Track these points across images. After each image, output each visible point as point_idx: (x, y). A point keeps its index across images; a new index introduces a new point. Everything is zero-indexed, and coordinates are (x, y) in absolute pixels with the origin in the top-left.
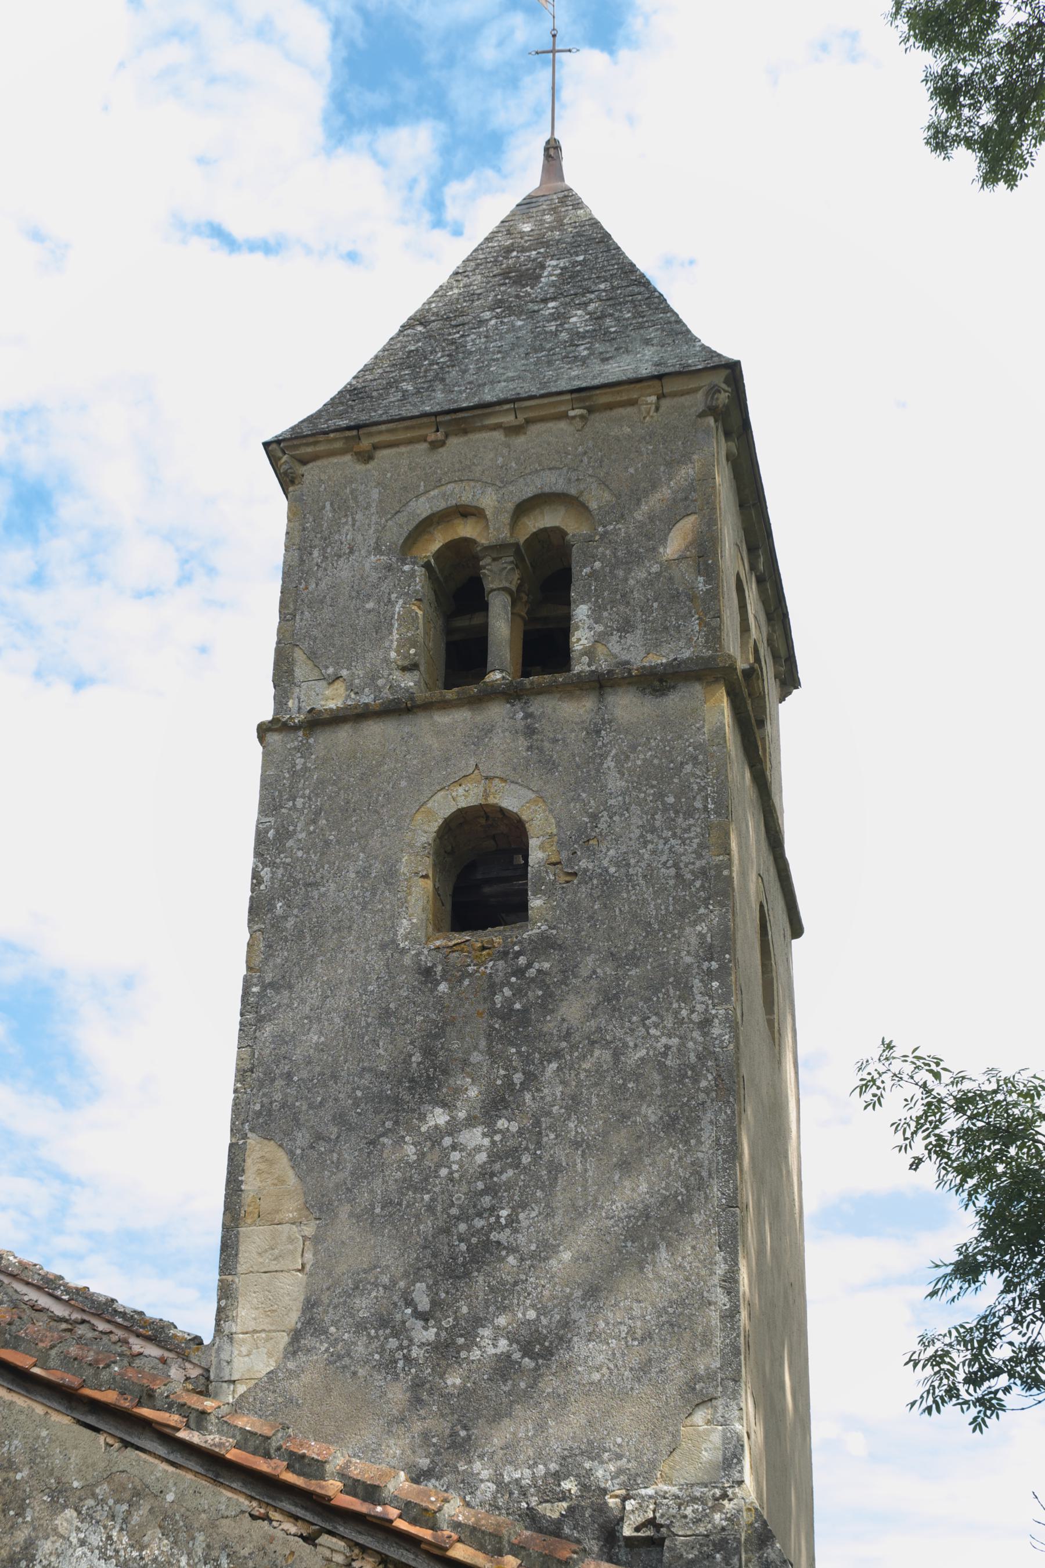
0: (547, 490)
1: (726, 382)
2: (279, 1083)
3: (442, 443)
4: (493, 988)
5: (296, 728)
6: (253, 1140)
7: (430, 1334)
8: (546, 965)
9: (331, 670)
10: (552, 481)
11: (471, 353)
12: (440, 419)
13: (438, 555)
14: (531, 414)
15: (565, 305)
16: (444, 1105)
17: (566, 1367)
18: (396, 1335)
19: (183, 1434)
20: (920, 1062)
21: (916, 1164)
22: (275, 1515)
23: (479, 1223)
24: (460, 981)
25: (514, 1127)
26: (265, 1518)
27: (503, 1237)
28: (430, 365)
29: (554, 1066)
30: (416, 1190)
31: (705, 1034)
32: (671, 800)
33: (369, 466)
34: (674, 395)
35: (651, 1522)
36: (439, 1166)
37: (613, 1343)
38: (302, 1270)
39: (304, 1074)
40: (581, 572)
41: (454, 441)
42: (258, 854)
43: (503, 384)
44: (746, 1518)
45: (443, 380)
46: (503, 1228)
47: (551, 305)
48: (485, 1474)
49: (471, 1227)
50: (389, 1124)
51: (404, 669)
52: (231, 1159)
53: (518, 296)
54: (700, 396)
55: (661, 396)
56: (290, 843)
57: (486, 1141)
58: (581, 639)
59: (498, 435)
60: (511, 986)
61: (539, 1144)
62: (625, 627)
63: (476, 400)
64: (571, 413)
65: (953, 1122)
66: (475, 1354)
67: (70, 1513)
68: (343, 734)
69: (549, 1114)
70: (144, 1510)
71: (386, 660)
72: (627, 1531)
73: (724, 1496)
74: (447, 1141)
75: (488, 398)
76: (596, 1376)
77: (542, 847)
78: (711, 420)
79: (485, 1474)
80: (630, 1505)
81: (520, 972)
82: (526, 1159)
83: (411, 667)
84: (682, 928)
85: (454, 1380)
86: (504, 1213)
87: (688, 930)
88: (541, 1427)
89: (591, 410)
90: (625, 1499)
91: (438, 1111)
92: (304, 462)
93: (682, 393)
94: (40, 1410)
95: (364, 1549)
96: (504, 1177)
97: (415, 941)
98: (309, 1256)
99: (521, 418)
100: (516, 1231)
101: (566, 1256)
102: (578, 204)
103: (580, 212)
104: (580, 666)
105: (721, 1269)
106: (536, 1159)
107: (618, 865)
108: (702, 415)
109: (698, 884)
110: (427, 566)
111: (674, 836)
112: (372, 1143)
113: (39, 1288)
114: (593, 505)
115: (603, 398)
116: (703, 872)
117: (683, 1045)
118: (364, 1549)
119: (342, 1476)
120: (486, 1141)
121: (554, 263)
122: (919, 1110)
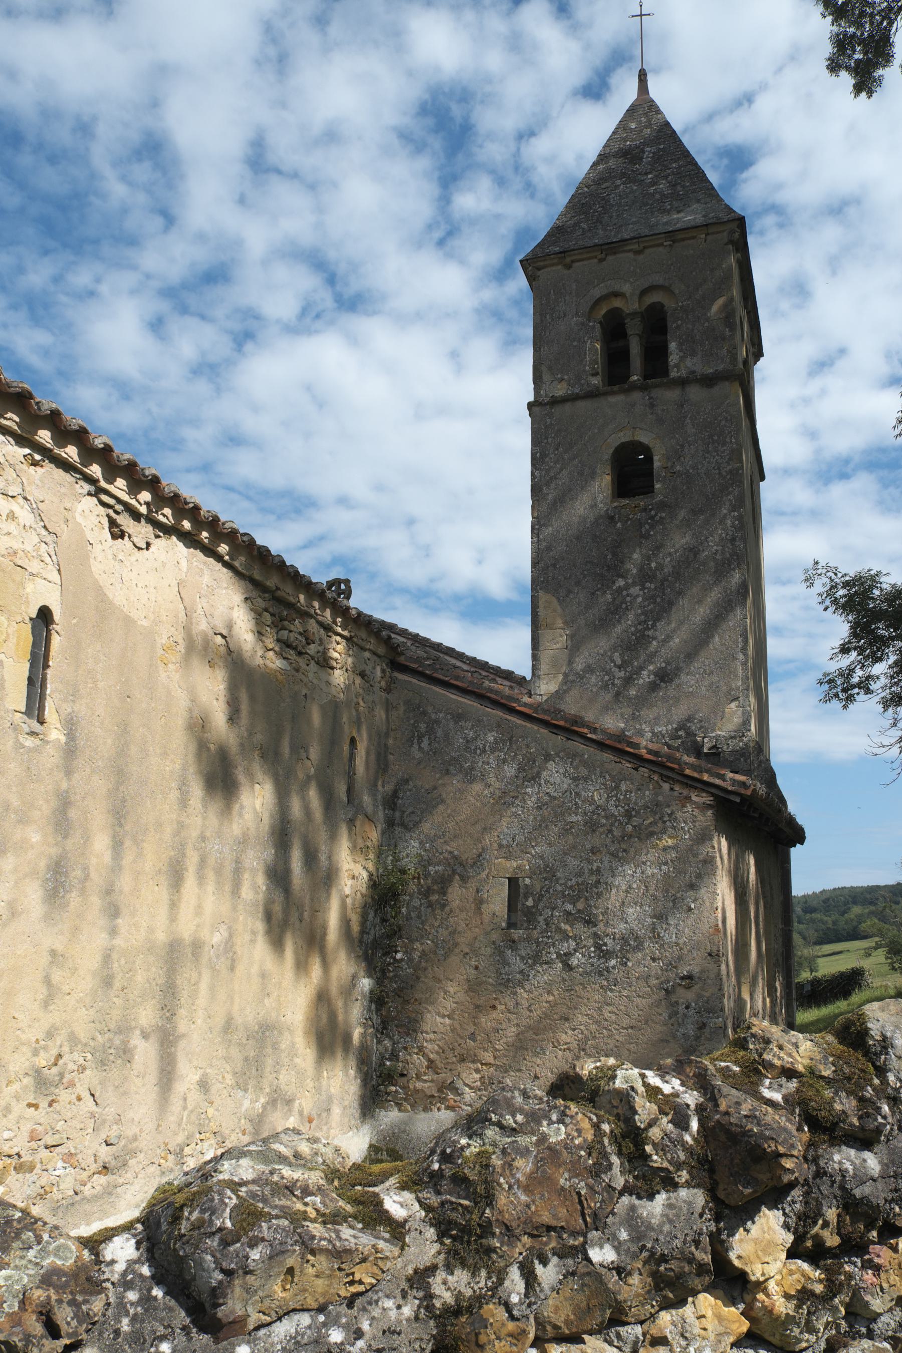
0: (655, 283)
1: (738, 227)
2: (551, 568)
3: (604, 260)
4: (641, 525)
5: (546, 404)
6: (541, 594)
7: (622, 674)
8: (664, 515)
9: (559, 376)
10: (658, 279)
11: (613, 206)
12: (603, 247)
13: (605, 316)
14: (646, 244)
15: (656, 176)
16: (622, 577)
17: (679, 686)
18: (607, 674)
19: (589, 736)
20: (828, 568)
21: (826, 609)
22: (623, 762)
23: (640, 627)
24: (626, 522)
25: (653, 586)
26: (620, 762)
27: (650, 633)
28: (594, 212)
29: (669, 559)
30: (612, 613)
31: (732, 545)
32: (716, 438)
33: (570, 271)
34: (713, 233)
35: (714, 747)
36: (622, 603)
37: (697, 676)
38: (566, 648)
39: (562, 564)
40: (672, 325)
41: (610, 258)
42: (533, 465)
43: (631, 226)
44: (751, 744)
45: (601, 222)
46: (650, 629)
47: (650, 176)
48: (647, 729)
49: (636, 629)
50: (599, 586)
51: (593, 375)
52: (532, 602)
53: (632, 171)
54: (725, 234)
55: (707, 234)
56: (547, 459)
57: (641, 593)
58: (673, 359)
59: (631, 255)
60: (649, 524)
61: (664, 594)
62: (693, 354)
63: (619, 237)
64: (665, 244)
65: (842, 592)
66: (641, 681)
67: (551, 762)
68: (568, 407)
69: (667, 580)
70: (577, 761)
71: (584, 371)
72: (705, 751)
73: (743, 736)
74: (625, 593)
75: (626, 236)
76: (691, 689)
77: (659, 460)
78: (730, 247)
79: (647, 729)
80: (706, 740)
81: (652, 518)
82: (658, 600)
83: (595, 374)
84: (722, 497)
85: (633, 692)
86: (650, 623)
87: (724, 498)
88: (669, 710)
89: (674, 241)
90: (704, 738)
91: (620, 580)
92: (539, 269)
93: (719, 232)
94: (536, 728)
95: (654, 771)
96: (649, 608)
97: (606, 504)
98: (569, 642)
99: (642, 246)
100: (656, 630)
101: (677, 640)
102: (658, 111)
103: (659, 116)
104: (674, 374)
105: (740, 645)
106: (663, 600)
107: (693, 468)
108: (726, 244)
109: (728, 477)
110: (600, 323)
111: (718, 455)
112: (593, 594)
113: (456, 658)
114: (677, 291)
115: (680, 236)
116: (731, 471)
117: (723, 549)
118: (654, 771)
119: (646, 748)
120: (641, 593)
121: (649, 149)
122: (828, 587)
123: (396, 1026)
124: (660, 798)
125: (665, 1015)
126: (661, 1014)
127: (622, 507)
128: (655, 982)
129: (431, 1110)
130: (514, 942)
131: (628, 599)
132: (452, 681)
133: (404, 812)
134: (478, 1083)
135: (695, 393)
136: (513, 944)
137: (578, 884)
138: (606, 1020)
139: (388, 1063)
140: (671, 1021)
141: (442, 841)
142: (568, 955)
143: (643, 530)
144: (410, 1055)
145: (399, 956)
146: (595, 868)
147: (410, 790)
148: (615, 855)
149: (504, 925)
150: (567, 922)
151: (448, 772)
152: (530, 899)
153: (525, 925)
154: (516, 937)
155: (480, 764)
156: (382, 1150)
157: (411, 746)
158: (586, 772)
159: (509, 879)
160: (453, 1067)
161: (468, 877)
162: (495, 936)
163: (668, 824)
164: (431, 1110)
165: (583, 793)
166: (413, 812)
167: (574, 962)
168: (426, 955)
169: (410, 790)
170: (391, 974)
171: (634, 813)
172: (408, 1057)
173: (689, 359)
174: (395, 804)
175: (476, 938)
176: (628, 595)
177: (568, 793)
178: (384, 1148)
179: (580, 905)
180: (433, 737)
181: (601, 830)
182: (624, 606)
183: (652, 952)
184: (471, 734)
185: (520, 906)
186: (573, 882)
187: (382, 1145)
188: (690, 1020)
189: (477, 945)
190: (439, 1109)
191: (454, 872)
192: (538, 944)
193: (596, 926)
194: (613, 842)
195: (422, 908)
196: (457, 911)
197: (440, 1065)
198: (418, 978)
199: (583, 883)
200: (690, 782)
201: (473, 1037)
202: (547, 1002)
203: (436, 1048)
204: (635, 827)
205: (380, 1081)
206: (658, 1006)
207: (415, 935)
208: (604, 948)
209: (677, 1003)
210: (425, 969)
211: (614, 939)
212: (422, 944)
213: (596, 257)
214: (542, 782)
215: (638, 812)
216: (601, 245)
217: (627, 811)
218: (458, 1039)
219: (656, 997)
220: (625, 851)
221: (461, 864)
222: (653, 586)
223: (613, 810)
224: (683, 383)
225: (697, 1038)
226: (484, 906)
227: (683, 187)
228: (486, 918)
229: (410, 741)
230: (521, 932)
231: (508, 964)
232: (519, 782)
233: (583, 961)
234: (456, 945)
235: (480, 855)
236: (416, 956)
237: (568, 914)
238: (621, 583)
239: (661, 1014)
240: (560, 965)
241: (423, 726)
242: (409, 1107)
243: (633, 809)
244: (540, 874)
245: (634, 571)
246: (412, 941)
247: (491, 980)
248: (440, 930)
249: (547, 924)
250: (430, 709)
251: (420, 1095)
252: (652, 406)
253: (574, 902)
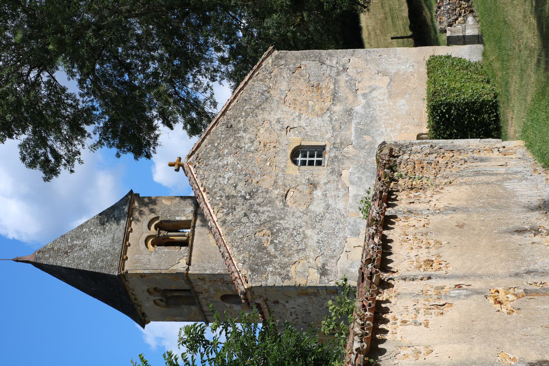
62: (184, 211)
68: (192, 258)
71: (177, 252)
173: (185, 212)
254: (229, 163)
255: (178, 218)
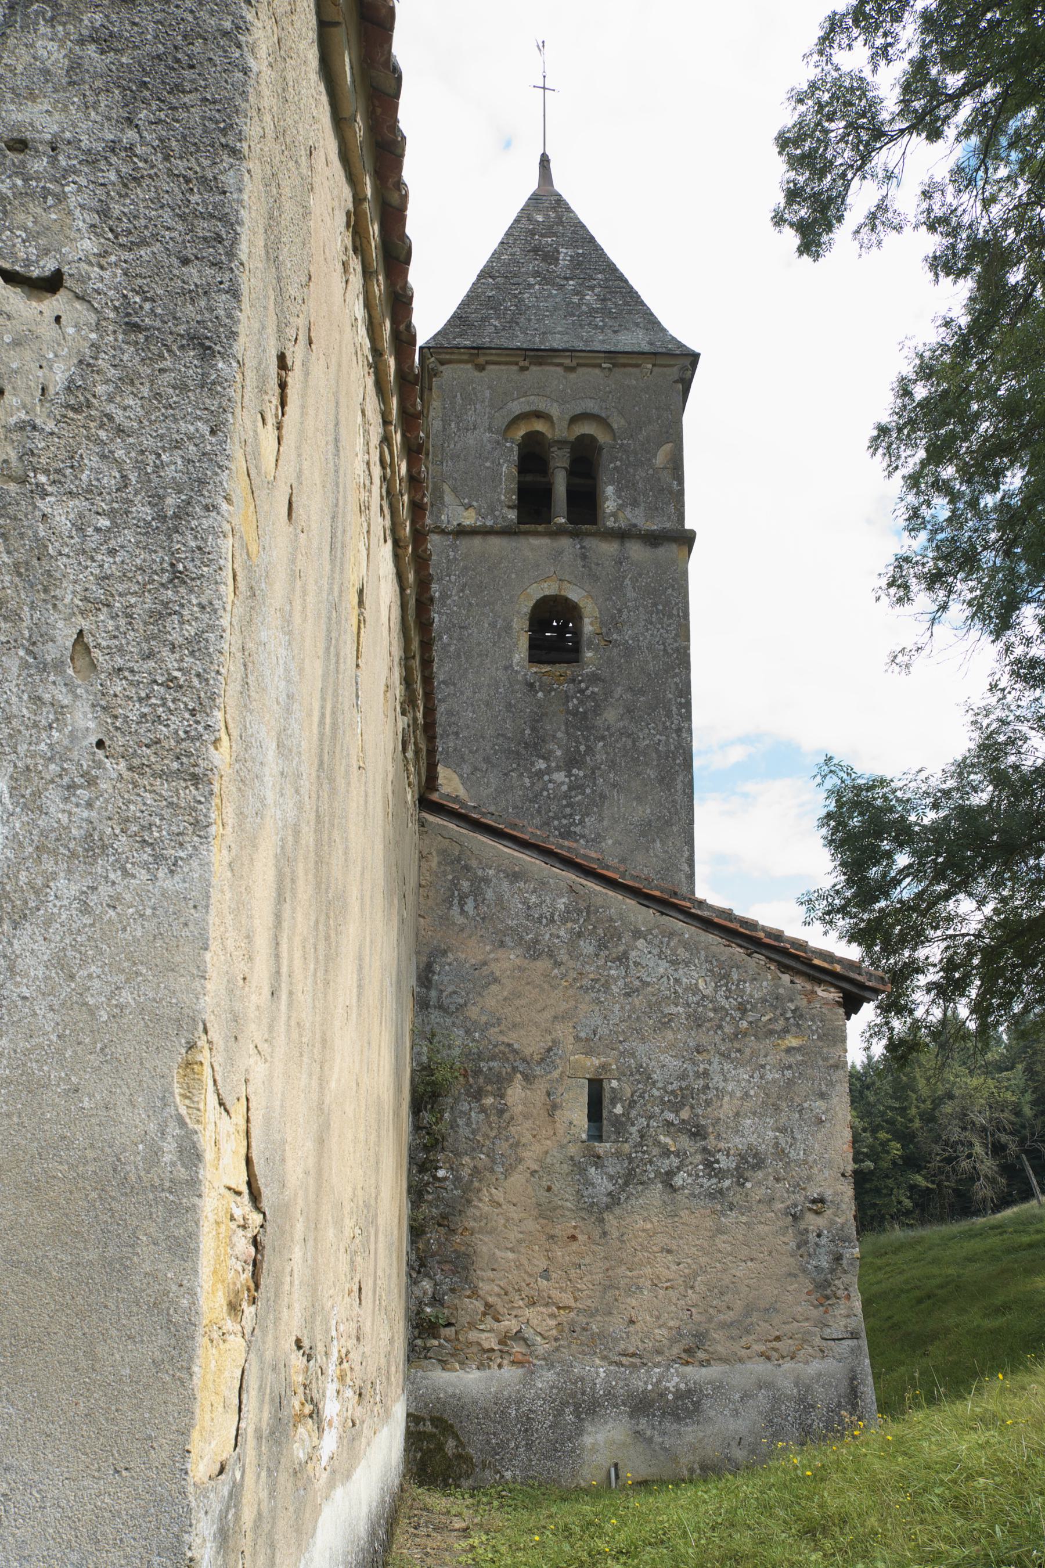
3: (527, 369)
4: (567, 698)
23: (564, 822)
24: (550, 692)
25: (581, 774)
27: (578, 829)
32: (660, 607)
33: (483, 374)
34: (661, 366)
36: (542, 790)
41: (534, 368)
56: (449, 602)
59: (560, 370)
61: (595, 784)
62: (635, 504)
67: (642, 940)
68: (477, 541)
71: (499, 500)
74: (546, 778)
75: (555, 345)
82: (588, 791)
89: (614, 365)
94: (620, 897)
95: (771, 960)
101: (610, 842)
108: (676, 382)
114: (615, 426)
115: (623, 360)
123: (439, 1262)
124: (781, 991)
125: (793, 1245)
126: (787, 1244)
127: (544, 674)
128: (781, 1206)
129: (489, 1367)
130: (599, 1157)
131: (551, 786)
132: (507, 830)
133: (442, 991)
134: (554, 1332)
135: (636, 551)
136: (597, 1160)
137: (681, 1089)
138: (720, 1251)
139: (428, 1310)
140: (800, 1252)
141: (497, 1030)
142: (670, 1174)
143: (570, 704)
144: (460, 1297)
145: (441, 1173)
146: (701, 1070)
147: (450, 964)
148: (725, 1056)
149: (584, 1136)
150: (668, 1134)
151: (502, 944)
152: (619, 1106)
153: (613, 1137)
154: (601, 1152)
155: (547, 937)
156: (424, 1420)
157: (449, 909)
158: (687, 955)
159: (590, 1080)
160: (520, 1312)
161: (535, 1077)
162: (573, 1150)
163: (792, 1021)
164: (489, 1367)
165: (685, 980)
166: (455, 992)
167: (678, 1181)
168: (479, 1173)
169: (450, 964)
170: (430, 1197)
171: (749, 1007)
172: (457, 1301)
173: (629, 509)
174: (430, 981)
175: (547, 1152)
176: (550, 781)
177: (665, 979)
178: (427, 1417)
179: (685, 1114)
180: (480, 899)
181: (708, 1025)
182: (545, 793)
183: (776, 1171)
184: (534, 899)
185: (605, 1114)
186: (675, 1086)
187: (424, 1413)
188: (823, 1250)
189: (548, 1160)
190: (500, 1366)
191: (515, 1069)
192: (631, 1160)
193: (705, 1138)
194: (723, 1040)
195: (473, 1114)
196: (521, 1118)
197: (502, 1310)
198: (469, 1202)
199: (687, 1088)
200: (817, 975)
201: (546, 1274)
202: (644, 1230)
203: (497, 1289)
204: (751, 1023)
205: (416, 1333)
206: (784, 1235)
207: (463, 1146)
208: (716, 1166)
209: (806, 1230)
210: (479, 1190)
211: (728, 1155)
212: (473, 1158)
213: (517, 364)
214: (631, 963)
215: (754, 1007)
216: (526, 350)
217: (740, 1003)
218: (526, 1277)
219: (780, 1223)
220: (739, 1051)
221: (524, 1060)
222: (581, 774)
223: (723, 1002)
224: (623, 535)
225: (832, 1271)
226: (558, 1113)
227: (615, 304)
228: (561, 1129)
229: (448, 902)
230: (608, 1145)
231: (593, 1185)
232: (601, 963)
233: (689, 1181)
234: (520, 1160)
235: (550, 1050)
236: (465, 1173)
237: (669, 1124)
238: (541, 765)
239: (787, 1244)
240: (660, 1185)
241: (465, 885)
242: (457, 1365)
243: (748, 1002)
244: (631, 1075)
245: (559, 753)
246: (457, 1154)
247: (568, 1204)
248: (497, 1142)
249: (642, 1137)
250: (474, 863)
251: (475, 1349)
252: (584, 557)
253: (676, 1109)
254: (621, 711)
255: (610, 490)
